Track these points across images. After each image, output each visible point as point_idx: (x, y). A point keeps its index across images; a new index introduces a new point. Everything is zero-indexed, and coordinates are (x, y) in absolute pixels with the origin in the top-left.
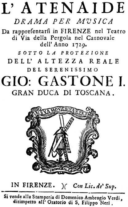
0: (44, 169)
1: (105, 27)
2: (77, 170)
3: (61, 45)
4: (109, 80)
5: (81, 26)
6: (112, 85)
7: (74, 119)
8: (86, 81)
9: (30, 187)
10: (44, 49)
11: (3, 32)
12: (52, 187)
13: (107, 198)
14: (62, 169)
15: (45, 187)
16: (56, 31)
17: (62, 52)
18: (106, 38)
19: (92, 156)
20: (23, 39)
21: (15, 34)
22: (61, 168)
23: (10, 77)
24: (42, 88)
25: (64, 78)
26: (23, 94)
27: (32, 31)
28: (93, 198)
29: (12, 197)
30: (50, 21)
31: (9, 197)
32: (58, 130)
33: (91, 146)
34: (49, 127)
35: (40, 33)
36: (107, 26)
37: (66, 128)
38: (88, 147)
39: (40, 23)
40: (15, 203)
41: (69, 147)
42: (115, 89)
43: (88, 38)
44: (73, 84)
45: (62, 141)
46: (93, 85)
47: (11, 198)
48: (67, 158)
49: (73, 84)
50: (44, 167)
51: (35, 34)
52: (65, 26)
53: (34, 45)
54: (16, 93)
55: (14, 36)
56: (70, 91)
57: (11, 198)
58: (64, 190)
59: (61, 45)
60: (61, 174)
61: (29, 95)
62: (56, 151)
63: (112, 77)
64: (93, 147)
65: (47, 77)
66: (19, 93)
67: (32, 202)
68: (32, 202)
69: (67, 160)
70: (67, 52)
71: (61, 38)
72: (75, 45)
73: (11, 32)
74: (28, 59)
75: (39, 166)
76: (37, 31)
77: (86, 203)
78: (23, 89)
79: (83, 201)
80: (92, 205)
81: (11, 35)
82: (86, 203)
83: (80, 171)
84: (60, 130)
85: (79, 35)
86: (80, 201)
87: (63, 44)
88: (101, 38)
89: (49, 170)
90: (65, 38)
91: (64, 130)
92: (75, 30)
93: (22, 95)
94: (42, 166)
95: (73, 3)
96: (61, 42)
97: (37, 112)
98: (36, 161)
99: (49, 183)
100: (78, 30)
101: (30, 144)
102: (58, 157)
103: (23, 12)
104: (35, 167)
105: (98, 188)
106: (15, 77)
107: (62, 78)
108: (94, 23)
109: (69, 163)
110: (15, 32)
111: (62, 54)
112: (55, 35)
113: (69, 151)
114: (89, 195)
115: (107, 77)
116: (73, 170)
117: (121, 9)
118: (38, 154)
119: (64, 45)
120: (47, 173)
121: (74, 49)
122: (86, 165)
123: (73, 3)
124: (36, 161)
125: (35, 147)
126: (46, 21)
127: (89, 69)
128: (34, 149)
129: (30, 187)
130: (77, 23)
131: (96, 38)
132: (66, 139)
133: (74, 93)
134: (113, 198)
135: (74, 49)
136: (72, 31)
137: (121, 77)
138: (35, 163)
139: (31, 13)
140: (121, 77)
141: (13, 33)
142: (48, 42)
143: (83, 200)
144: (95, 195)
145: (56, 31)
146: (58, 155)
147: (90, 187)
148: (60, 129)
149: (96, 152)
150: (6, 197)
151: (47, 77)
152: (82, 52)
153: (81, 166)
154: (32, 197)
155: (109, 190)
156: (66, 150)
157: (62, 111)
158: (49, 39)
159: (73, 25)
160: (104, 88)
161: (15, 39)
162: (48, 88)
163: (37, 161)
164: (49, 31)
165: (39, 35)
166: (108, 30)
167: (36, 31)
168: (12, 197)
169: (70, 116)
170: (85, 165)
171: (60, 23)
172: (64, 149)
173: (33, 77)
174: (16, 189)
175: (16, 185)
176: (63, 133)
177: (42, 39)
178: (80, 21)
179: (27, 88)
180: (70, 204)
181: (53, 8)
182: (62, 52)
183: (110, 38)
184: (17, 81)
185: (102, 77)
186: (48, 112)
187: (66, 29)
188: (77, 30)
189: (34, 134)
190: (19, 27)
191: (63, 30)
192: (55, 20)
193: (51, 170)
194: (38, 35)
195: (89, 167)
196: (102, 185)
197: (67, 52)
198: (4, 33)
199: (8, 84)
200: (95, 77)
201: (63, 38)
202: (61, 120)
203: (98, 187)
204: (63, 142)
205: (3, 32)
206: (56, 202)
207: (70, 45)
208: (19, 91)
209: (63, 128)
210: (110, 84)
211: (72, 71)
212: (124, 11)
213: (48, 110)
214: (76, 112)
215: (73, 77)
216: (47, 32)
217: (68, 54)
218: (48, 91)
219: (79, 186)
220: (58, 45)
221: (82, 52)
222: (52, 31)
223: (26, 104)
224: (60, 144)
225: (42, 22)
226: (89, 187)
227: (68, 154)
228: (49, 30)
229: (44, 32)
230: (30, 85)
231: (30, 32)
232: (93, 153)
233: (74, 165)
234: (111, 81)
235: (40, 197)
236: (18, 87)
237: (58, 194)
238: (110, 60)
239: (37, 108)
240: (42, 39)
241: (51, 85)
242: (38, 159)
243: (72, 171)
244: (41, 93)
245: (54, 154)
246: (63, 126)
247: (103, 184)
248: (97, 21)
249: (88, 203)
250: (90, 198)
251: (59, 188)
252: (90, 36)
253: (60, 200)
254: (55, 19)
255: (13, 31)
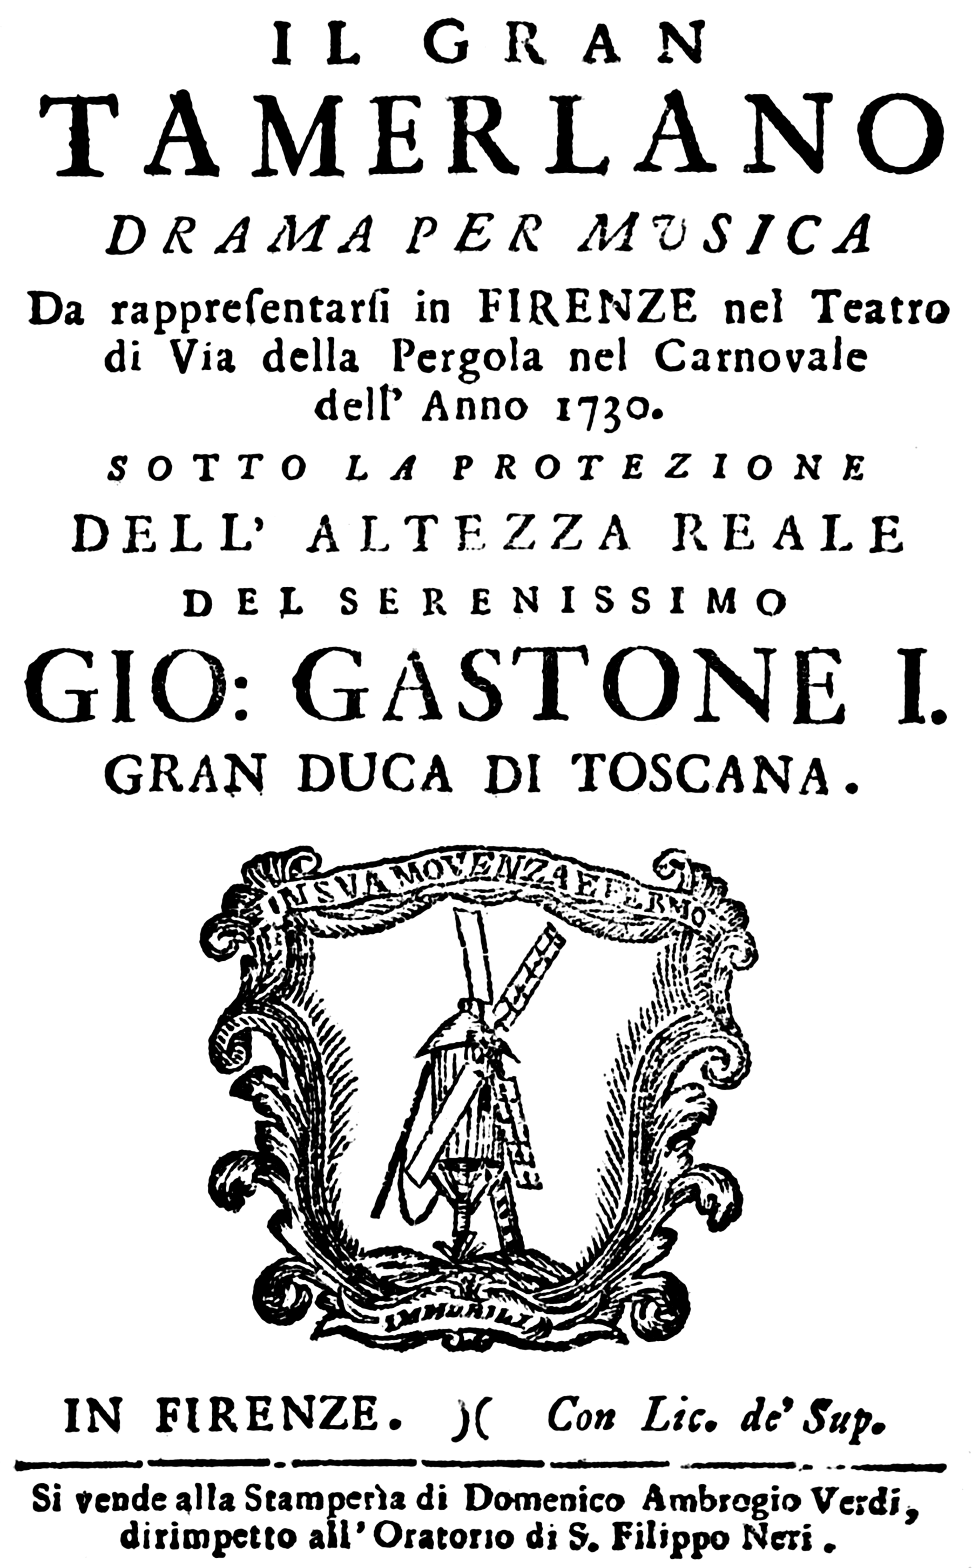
0: (343, 1314)
1: (798, 278)
2: (589, 1320)
3: (479, 411)
4: (817, 674)
5: (606, 270)
6: (839, 718)
7: (563, 942)
8: (641, 683)
9: (215, 1428)
10: (329, 444)
11: (36, 308)
12: (384, 1425)
13: (809, 1501)
14: (476, 1311)
15: (326, 1424)
16: (439, 309)
17: (464, 462)
18: (807, 358)
19: (702, 1210)
20: (816, 764)
21: (128, 331)
22: (466, 1305)
23: (88, 657)
24: (331, 739)
25: (482, 665)
26: (187, 783)
27: (257, 308)
28: (707, 1503)
29: (93, 1503)
30: (390, 235)
31: (69, 1502)
32: (449, 1024)
33: (688, 1136)
34: (380, 997)
35: (315, 319)
36: (825, 269)
37: (503, 1009)
38: (671, 1144)
39: (314, 247)
40: (429, 1506)
41: (524, 1149)
42: (868, 728)
43: (670, 360)
44: (550, 711)
45: (474, 1105)
46: (700, 713)
47: (83, 1509)
48: (514, 1228)
49: (550, 711)
50: (338, 1295)
51: (281, 328)
52: (500, 268)
53: (273, 411)
54: (136, 779)
55: (121, 342)
56: (533, 759)
57: (83, 1509)
58: (472, 1448)
59: (479, 411)
60: (464, 1346)
61: (760, 788)
62: (430, 1176)
63: (834, 654)
64: (707, 1147)
65: (357, 657)
66: (157, 772)
67: (261, 1538)
68: (261, 1538)
69: (514, 1247)
70: (502, 457)
71: (469, 356)
72: (578, 413)
73: (97, 314)
74: (230, 518)
75: (300, 1289)
76: (294, 308)
77: (645, 1539)
78: (189, 744)
79: (618, 1526)
80: (688, 1551)
81: (99, 333)
82: (645, 1539)
83: (613, 1323)
84: (465, 1023)
85: (594, 337)
86: (600, 1526)
87: (491, 405)
88: (769, 361)
89: (376, 1320)
90: (494, 359)
91: (490, 1020)
92: (579, 298)
93: (178, 788)
94: (327, 1290)
95: (256, 174)
96: (470, 383)
97: (292, 886)
98: (283, 1253)
99: (358, 1399)
100: (606, 295)
101: (237, 1127)
102: (442, 1224)
103: (155, 168)
104: (272, 1296)
105: (756, 1427)
106: (123, 659)
107: (467, 662)
108: (715, 243)
109: (530, 1265)
110: (126, 314)
111: (458, 476)
112: (429, 336)
113: (526, 1175)
114: (674, 1482)
115: (802, 658)
116: (556, 1319)
117: (817, 696)
118: (293, 1198)
119: (493, 408)
120: (368, 1341)
121: (570, 441)
122: (658, 1283)
123: (256, 174)
124: (283, 1253)
125: (276, 1152)
126: (362, 231)
127: (721, 596)
128: (266, 1163)
129: (215, 1428)
130: (584, 248)
131: (730, 361)
132: (509, 1085)
133: (559, 776)
134: (848, 1500)
135: (570, 441)
136: (560, 308)
137: (912, 658)
138: (279, 1265)
139: (214, 171)
140: (912, 658)
141: (117, 321)
142: (370, 390)
143: (620, 1516)
144: (719, 1482)
145: (439, 311)
146: (444, 1208)
147: (685, 1421)
148: (456, 1017)
149: (729, 1180)
150: (45, 1501)
151: (357, 657)
152: (630, 458)
153: (617, 1288)
154: (240, 1500)
155: (831, 1447)
156: (507, 1167)
157: (481, 885)
158: (376, 367)
159: (556, 266)
160: (779, 735)
161: (129, 362)
162: (361, 737)
163: (290, 1249)
164: (385, 304)
165: (306, 336)
166: (820, 298)
167: (288, 303)
168: (93, 1503)
169: (538, 918)
170: (648, 1284)
171: (461, 246)
172: (487, 1166)
173: (263, 652)
174: (104, 1445)
175: (100, 1422)
176: (473, 1053)
177: (324, 363)
178: (603, 233)
179: (220, 737)
180: (539, 1544)
181: (386, 134)
182: (464, 462)
183: (830, 361)
184: (142, 683)
185: (767, 653)
186: (374, 890)
187: (514, 293)
188: (594, 302)
189: (263, 1053)
190: (153, 276)
191: (493, 297)
192: (425, 225)
193: (390, 1319)
194: (298, 335)
195: (676, 1298)
196: (780, 1408)
197: (502, 457)
198: (501, 785)
199: (71, 707)
200: (708, 655)
201: (481, 357)
202: (473, 952)
203: (750, 1423)
204: (484, 1105)
205: (36, 308)
206: (435, 1538)
207: (543, 409)
208: (157, 758)
209: (482, 1004)
210: (821, 705)
211: (568, 609)
212: (842, 709)
213: (370, 876)
214: (582, 885)
215: (550, 655)
216: (364, 312)
217: (512, 476)
218: (372, 757)
219: (586, 1421)
220: (452, 410)
221: (630, 458)
222: (403, 309)
223: (213, 842)
224: (453, 1140)
225: (332, 237)
226: (678, 1426)
227: (520, 1195)
228: (380, 297)
229: (348, 312)
230: (241, 715)
231: (243, 312)
232: (706, 1189)
233: (563, 1280)
234: (829, 686)
235: (300, 1496)
236: (149, 731)
237: (437, 1476)
238: (831, 520)
239: (285, 856)
240: (324, 363)
241: (390, 716)
242: (296, 1234)
243: (545, 1327)
244: (318, 774)
245: (418, 1199)
246: (481, 992)
247: (788, 1403)
248: (740, 233)
249: (658, 1539)
250: (685, 1502)
251: (429, 1434)
252: (681, 344)
253: (456, 1516)
254: (420, 221)
255: (118, 307)
